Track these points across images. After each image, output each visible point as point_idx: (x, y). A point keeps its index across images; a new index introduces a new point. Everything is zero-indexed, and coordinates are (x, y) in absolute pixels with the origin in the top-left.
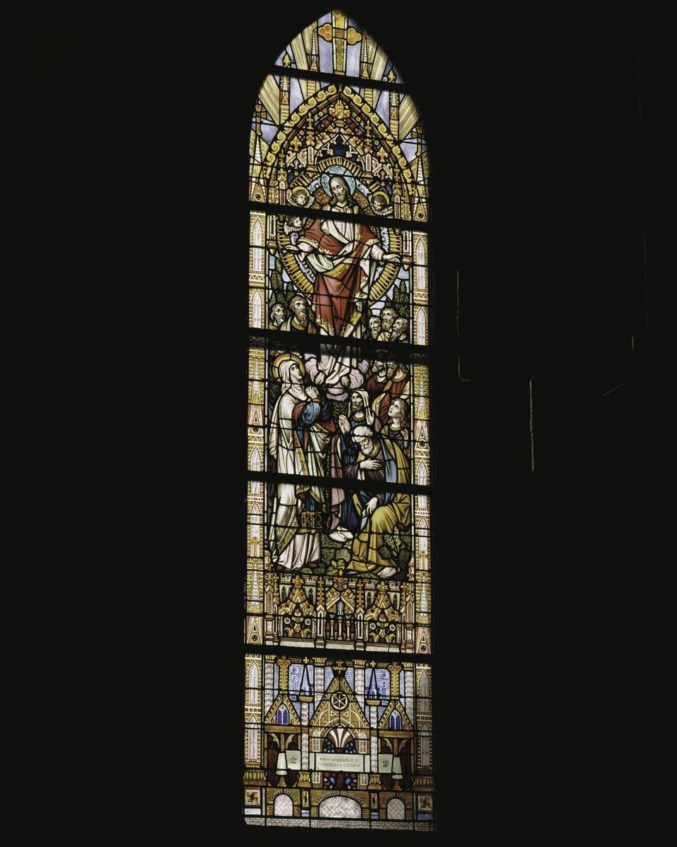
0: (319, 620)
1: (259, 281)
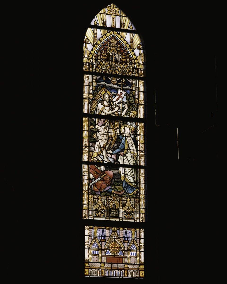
0: (107, 212)
1: (87, 97)
